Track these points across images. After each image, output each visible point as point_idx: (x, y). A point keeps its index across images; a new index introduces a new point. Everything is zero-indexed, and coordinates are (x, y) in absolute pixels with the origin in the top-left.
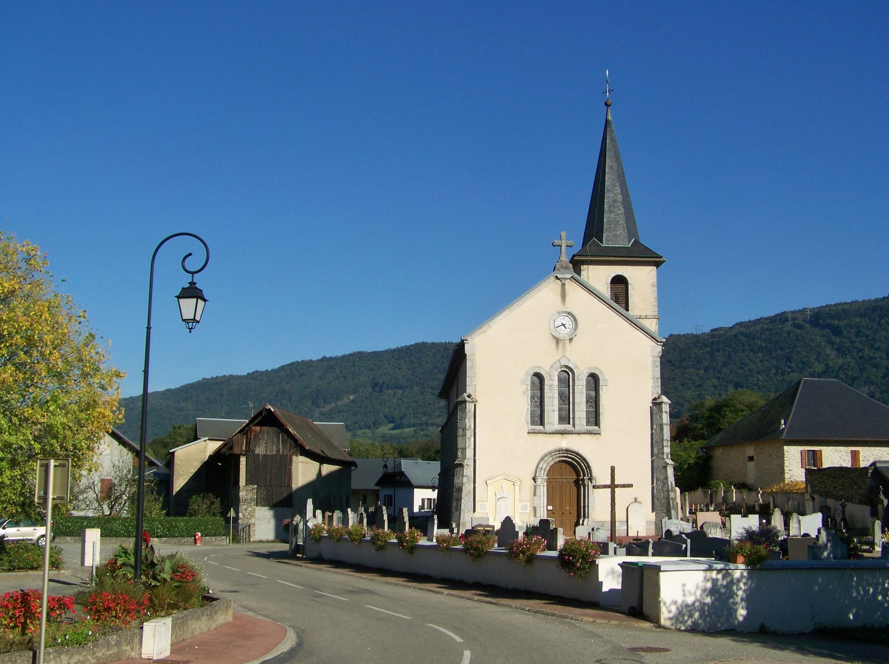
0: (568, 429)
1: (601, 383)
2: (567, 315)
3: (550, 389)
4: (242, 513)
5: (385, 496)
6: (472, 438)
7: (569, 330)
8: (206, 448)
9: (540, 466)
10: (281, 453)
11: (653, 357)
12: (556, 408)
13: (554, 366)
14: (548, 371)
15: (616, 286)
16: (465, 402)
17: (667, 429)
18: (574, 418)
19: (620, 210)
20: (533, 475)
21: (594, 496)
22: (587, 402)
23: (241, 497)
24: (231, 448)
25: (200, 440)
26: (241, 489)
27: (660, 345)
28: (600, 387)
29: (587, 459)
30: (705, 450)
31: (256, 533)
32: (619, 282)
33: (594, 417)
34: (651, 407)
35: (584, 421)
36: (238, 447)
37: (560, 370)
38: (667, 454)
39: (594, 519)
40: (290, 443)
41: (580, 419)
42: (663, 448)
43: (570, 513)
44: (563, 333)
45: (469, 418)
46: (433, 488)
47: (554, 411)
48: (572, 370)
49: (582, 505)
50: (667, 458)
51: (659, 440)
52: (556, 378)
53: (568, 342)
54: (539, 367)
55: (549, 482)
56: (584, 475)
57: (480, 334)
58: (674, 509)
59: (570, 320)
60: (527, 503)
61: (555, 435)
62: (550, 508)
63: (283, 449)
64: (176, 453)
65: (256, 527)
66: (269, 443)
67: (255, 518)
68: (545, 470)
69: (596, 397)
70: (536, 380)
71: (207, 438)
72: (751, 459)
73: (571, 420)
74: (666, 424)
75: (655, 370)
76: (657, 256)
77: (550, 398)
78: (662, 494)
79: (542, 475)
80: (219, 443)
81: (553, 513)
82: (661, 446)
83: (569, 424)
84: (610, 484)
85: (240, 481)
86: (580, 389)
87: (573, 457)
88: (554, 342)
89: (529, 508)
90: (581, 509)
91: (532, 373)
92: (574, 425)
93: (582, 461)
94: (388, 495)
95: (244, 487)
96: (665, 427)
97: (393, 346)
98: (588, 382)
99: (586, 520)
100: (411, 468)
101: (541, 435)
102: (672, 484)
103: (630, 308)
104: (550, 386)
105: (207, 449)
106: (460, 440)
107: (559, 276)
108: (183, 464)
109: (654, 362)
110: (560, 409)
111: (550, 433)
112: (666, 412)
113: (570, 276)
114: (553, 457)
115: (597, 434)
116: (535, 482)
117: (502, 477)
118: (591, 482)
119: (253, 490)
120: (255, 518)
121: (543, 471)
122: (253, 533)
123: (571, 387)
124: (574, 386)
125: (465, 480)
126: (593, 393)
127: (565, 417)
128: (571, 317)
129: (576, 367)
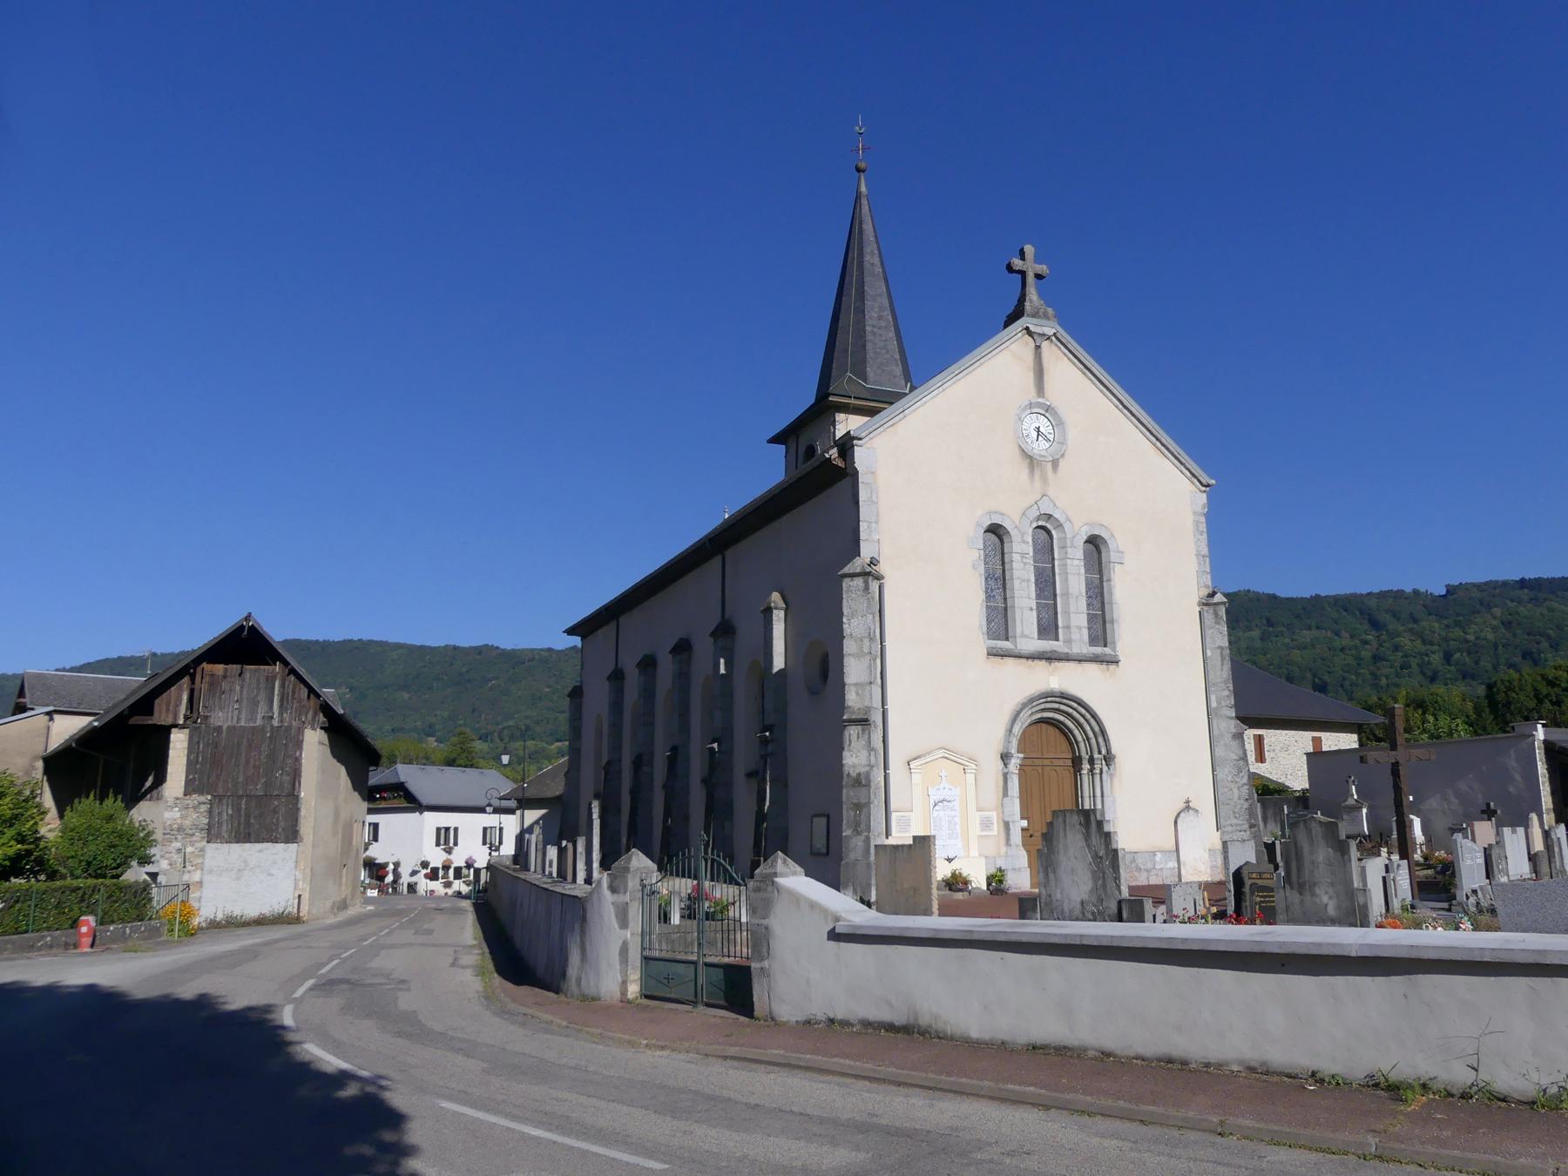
3: (1022, 562)
10: (276, 723)
11: (1195, 513)
13: (1028, 513)
21: (1114, 798)
25: (32, 713)
27: (1205, 492)
33: (1101, 626)
36: (168, 710)
37: (1035, 525)
54: (1002, 514)
59: (1046, 420)
60: (990, 813)
61: (1037, 662)
63: (281, 714)
65: (204, 890)
66: (245, 702)
75: (1199, 540)
77: (1023, 581)
78: (1236, 791)
81: (1031, 836)
83: (1057, 639)
86: (1076, 566)
87: (1070, 710)
89: (995, 825)
93: (1087, 721)
101: (1010, 661)
107: (1032, 328)
109: (1197, 523)
117: (941, 753)
119: (202, 806)
127: (1048, 628)
129: (1068, 519)
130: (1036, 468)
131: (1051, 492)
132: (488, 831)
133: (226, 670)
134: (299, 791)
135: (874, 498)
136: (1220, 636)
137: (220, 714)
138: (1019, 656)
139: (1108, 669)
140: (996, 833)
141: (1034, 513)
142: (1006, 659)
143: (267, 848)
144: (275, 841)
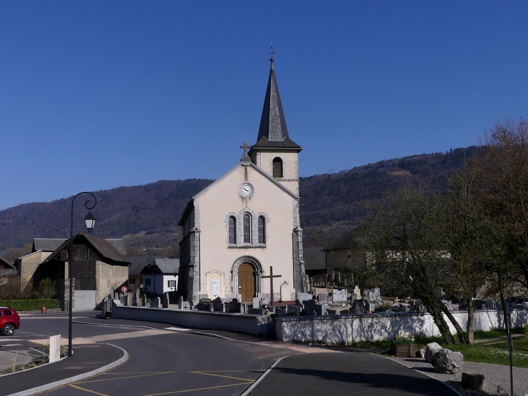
0: (249, 245)
1: (266, 221)
2: (248, 185)
4: (67, 294)
5: (146, 280)
6: (198, 251)
7: (249, 193)
8: (40, 256)
9: (235, 265)
12: (243, 234)
14: (238, 215)
15: (276, 163)
16: (194, 232)
17: (301, 245)
18: (252, 240)
19: (278, 121)
20: (231, 270)
21: (263, 281)
22: (259, 231)
23: (66, 285)
24: (59, 257)
26: (65, 280)
28: (266, 223)
29: (259, 261)
30: (325, 252)
31: (75, 305)
32: (278, 161)
33: (263, 239)
34: (292, 233)
35: (257, 241)
37: (244, 214)
38: (301, 258)
39: (263, 292)
40: (95, 254)
41: (255, 240)
42: (299, 255)
43: (251, 290)
44: (246, 194)
45: (196, 241)
46: (175, 275)
47: (241, 236)
48: (251, 214)
49: (257, 285)
50: (301, 260)
51: (297, 250)
52: (242, 218)
53: (248, 199)
54: (234, 213)
55: (239, 273)
56: (258, 270)
57: (202, 196)
58: (306, 287)
62: (240, 287)
64: (22, 260)
65: (75, 302)
67: (74, 297)
68: (237, 267)
69: (264, 228)
70: (232, 220)
71: (41, 250)
72: (349, 257)
73: (251, 240)
74: (301, 242)
76: (298, 146)
78: (299, 278)
79: (235, 270)
80: (50, 254)
81: (242, 290)
82: (298, 254)
83: (250, 243)
84: (270, 275)
85: (65, 276)
88: (241, 199)
90: (256, 288)
91: (229, 216)
92: (252, 243)
93: (256, 262)
94: (148, 279)
95: (67, 279)
96: (300, 243)
97: (144, 183)
98: (259, 221)
99: (259, 293)
100: (162, 264)
101: (234, 249)
102: (304, 273)
103: (283, 175)
104: (239, 223)
105: (41, 257)
106: (192, 252)
107: (243, 164)
108: (27, 266)
110: (245, 235)
111: (239, 248)
112: (300, 236)
113: (249, 164)
114: (241, 260)
115: (264, 248)
116: (232, 274)
117: (214, 272)
118: (262, 273)
120: (74, 297)
121: (236, 268)
122: (73, 305)
123: (250, 223)
124: (252, 222)
125: (195, 274)
126: (262, 226)
127: (247, 239)
128: (250, 186)
129: (253, 212)
130: (244, 201)
131: (248, 206)
132: (170, 282)
133: (76, 246)
134: (96, 277)
135: (199, 213)
136: (97, 287)
137: (76, 257)
138: (237, 248)
139: (263, 249)
140: (229, 289)
141: (243, 211)
142: (233, 249)
143: (89, 291)
144: (91, 290)
